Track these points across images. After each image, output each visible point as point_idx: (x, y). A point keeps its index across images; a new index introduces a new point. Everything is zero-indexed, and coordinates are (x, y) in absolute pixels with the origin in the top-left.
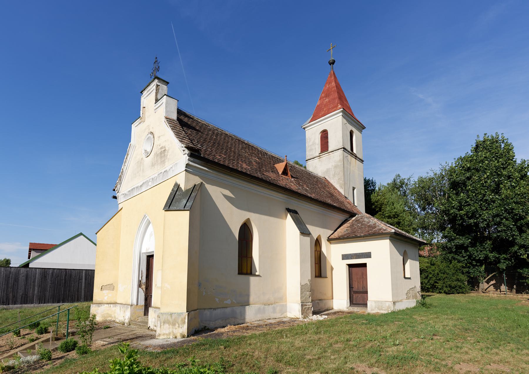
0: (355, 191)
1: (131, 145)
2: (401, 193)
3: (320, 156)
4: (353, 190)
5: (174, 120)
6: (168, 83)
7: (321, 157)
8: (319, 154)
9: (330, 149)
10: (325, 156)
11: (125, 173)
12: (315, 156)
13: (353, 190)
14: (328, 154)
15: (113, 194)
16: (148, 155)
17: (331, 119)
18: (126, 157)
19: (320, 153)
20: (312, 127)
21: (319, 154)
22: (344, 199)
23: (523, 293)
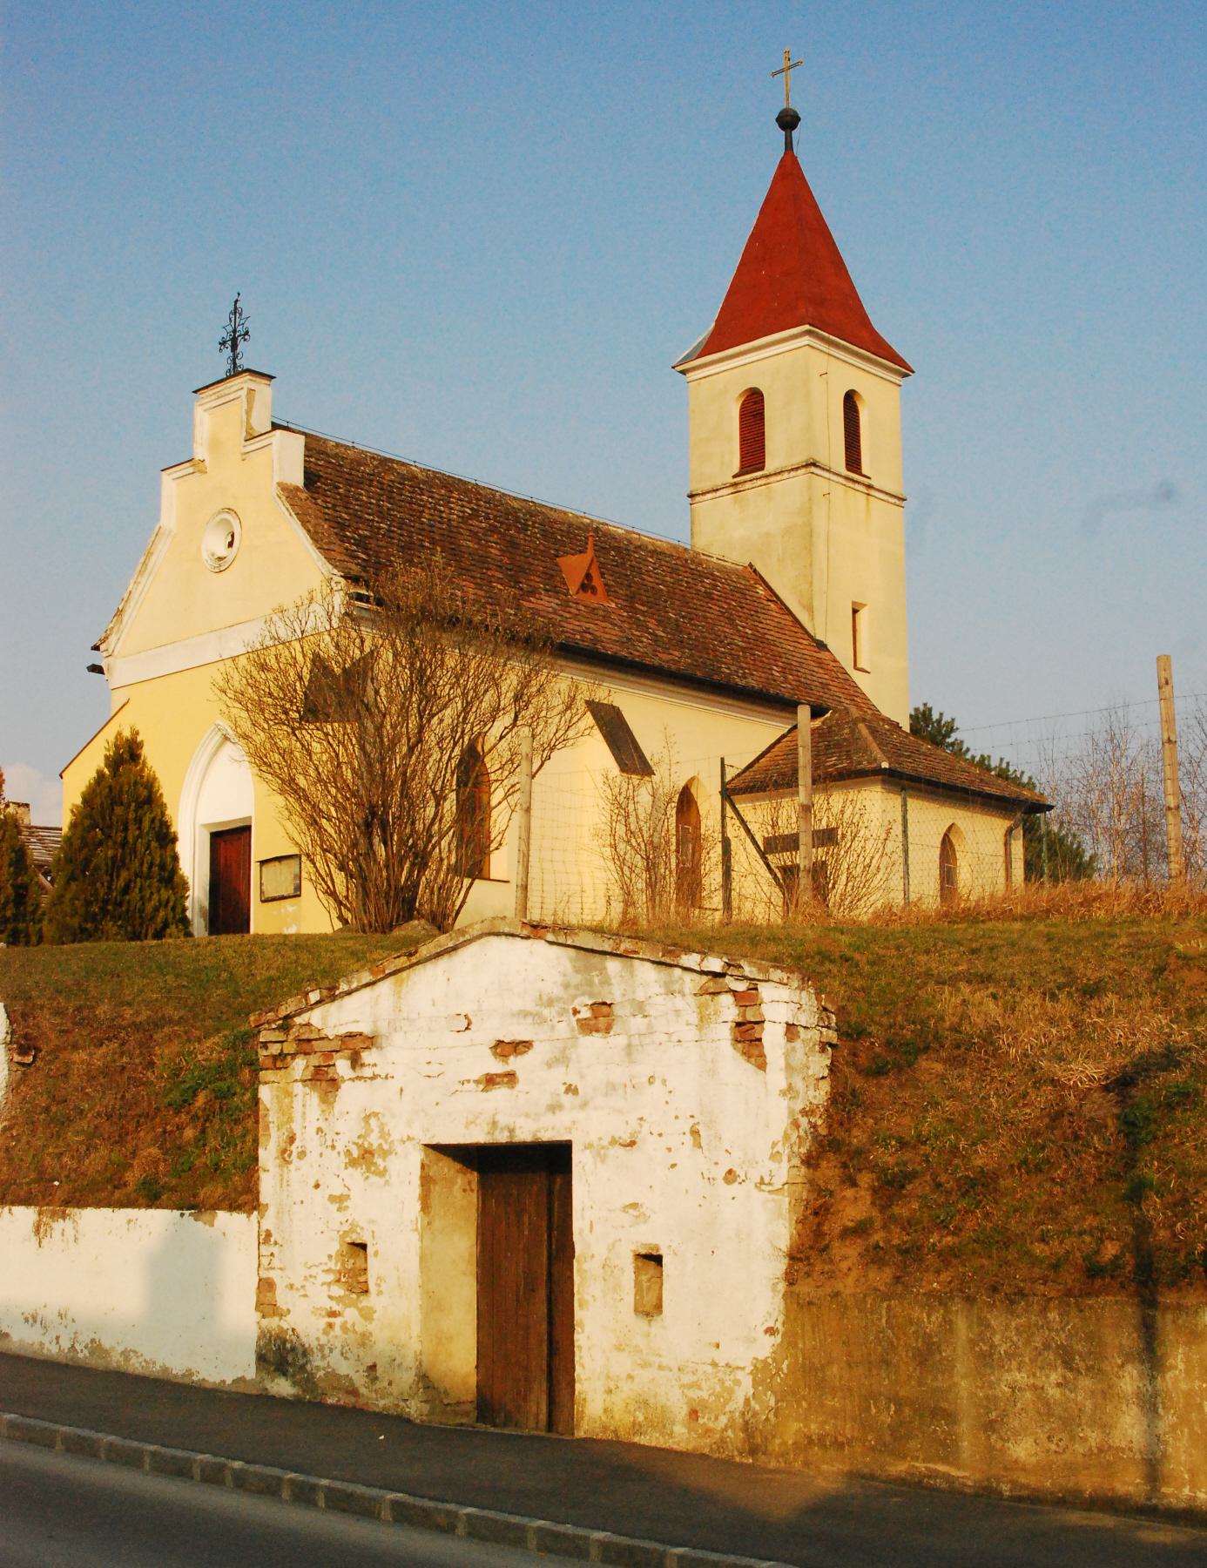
0: (861, 616)
1: (162, 531)
2: (203, 1131)
3: (735, 485)
4: (855, 612)
5: (297, 489)
6: (271, 377)
7: (740, 488)
8: (734, 477)
9: (771, 465)
10: (755, 492)
11: (137, 602)
12: (718, 483)
13: (855, 612)
14: (763, 481)
15: (96, 658)
16: (222, 568)
17: (775, 352)
18: (142, 560)
19: (736, 470)
20: (708, 373)
21: (734, 477)
22: (810, 651)
23: (12, 869)
